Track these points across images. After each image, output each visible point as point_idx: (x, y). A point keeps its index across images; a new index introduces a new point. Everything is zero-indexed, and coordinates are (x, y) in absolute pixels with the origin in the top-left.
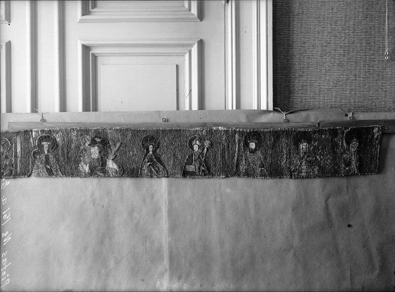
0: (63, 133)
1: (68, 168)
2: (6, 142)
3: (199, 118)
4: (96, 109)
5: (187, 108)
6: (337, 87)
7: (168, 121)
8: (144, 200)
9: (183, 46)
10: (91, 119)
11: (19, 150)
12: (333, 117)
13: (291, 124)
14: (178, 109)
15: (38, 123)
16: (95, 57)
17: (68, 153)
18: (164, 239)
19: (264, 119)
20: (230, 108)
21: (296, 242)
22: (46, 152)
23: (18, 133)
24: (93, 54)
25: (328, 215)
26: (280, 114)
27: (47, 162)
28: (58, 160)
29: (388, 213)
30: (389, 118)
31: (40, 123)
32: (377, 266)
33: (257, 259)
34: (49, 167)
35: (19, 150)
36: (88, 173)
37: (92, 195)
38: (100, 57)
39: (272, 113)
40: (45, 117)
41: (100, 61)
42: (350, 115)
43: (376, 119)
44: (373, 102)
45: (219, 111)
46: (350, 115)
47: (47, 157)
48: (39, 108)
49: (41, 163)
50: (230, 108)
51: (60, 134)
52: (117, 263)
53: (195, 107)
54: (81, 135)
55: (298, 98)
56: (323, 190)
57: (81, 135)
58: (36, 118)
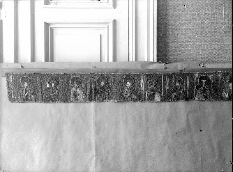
0: (214, 75)
1: (216, 95)
2: (181, 79)
3: (114, 66)
4: (52, 61)
5: (106, 61)
6: (195, 49)
7: (96, 68)
8: (81, 115)
9: (105, 23)
10: (49, 66)
11: (188, 84)
12: (193, 66)
13: (168, 70)
14: (101, 61)
15: (19, 68)
16: (52, 30)
17: (216, 86)
18: (92, 138)
19: (151, 67)
20: (131, 61)
21: (170, 140)
22: (204, 86)
23: (188, 74)
24: (51, 28)
25: (188, 124)
26: (161, 64)
27: (204, 91)
28: (210, 90)
29: (223, 123)
30: (225, 67)
31: (20, 68)
32: (217, 155)
33: (147, 150)
34: (205, 94)
35: (188, 84)
36: (228, 98)
37: (50, 112)
38: (57, 30)
39: (156, 64)
40: (23, 65)
41: (55, 32)
42: (202, 65)
43: (217, 67)
44: (216, 57)
45: (125, 62)
46: (202, 65)
47: (204, 88)
48: (19, 59)
49: (201, 92)
50: (131, 61)
51: (212, 75)
52: (65, 152)
53: (111, 60)
54: (224, 76)
55: (172, 54)
56: (185, 110)
57: (224, 76)
58: (18, 66)
